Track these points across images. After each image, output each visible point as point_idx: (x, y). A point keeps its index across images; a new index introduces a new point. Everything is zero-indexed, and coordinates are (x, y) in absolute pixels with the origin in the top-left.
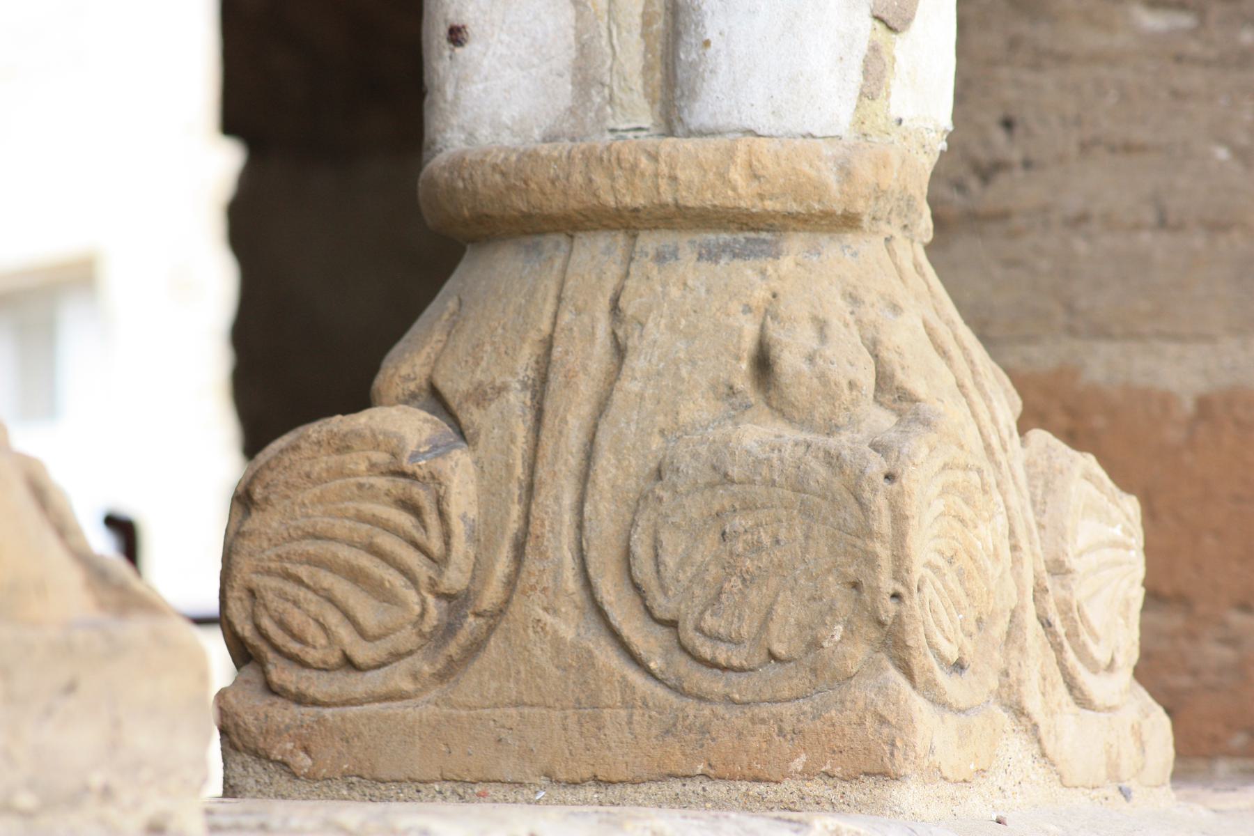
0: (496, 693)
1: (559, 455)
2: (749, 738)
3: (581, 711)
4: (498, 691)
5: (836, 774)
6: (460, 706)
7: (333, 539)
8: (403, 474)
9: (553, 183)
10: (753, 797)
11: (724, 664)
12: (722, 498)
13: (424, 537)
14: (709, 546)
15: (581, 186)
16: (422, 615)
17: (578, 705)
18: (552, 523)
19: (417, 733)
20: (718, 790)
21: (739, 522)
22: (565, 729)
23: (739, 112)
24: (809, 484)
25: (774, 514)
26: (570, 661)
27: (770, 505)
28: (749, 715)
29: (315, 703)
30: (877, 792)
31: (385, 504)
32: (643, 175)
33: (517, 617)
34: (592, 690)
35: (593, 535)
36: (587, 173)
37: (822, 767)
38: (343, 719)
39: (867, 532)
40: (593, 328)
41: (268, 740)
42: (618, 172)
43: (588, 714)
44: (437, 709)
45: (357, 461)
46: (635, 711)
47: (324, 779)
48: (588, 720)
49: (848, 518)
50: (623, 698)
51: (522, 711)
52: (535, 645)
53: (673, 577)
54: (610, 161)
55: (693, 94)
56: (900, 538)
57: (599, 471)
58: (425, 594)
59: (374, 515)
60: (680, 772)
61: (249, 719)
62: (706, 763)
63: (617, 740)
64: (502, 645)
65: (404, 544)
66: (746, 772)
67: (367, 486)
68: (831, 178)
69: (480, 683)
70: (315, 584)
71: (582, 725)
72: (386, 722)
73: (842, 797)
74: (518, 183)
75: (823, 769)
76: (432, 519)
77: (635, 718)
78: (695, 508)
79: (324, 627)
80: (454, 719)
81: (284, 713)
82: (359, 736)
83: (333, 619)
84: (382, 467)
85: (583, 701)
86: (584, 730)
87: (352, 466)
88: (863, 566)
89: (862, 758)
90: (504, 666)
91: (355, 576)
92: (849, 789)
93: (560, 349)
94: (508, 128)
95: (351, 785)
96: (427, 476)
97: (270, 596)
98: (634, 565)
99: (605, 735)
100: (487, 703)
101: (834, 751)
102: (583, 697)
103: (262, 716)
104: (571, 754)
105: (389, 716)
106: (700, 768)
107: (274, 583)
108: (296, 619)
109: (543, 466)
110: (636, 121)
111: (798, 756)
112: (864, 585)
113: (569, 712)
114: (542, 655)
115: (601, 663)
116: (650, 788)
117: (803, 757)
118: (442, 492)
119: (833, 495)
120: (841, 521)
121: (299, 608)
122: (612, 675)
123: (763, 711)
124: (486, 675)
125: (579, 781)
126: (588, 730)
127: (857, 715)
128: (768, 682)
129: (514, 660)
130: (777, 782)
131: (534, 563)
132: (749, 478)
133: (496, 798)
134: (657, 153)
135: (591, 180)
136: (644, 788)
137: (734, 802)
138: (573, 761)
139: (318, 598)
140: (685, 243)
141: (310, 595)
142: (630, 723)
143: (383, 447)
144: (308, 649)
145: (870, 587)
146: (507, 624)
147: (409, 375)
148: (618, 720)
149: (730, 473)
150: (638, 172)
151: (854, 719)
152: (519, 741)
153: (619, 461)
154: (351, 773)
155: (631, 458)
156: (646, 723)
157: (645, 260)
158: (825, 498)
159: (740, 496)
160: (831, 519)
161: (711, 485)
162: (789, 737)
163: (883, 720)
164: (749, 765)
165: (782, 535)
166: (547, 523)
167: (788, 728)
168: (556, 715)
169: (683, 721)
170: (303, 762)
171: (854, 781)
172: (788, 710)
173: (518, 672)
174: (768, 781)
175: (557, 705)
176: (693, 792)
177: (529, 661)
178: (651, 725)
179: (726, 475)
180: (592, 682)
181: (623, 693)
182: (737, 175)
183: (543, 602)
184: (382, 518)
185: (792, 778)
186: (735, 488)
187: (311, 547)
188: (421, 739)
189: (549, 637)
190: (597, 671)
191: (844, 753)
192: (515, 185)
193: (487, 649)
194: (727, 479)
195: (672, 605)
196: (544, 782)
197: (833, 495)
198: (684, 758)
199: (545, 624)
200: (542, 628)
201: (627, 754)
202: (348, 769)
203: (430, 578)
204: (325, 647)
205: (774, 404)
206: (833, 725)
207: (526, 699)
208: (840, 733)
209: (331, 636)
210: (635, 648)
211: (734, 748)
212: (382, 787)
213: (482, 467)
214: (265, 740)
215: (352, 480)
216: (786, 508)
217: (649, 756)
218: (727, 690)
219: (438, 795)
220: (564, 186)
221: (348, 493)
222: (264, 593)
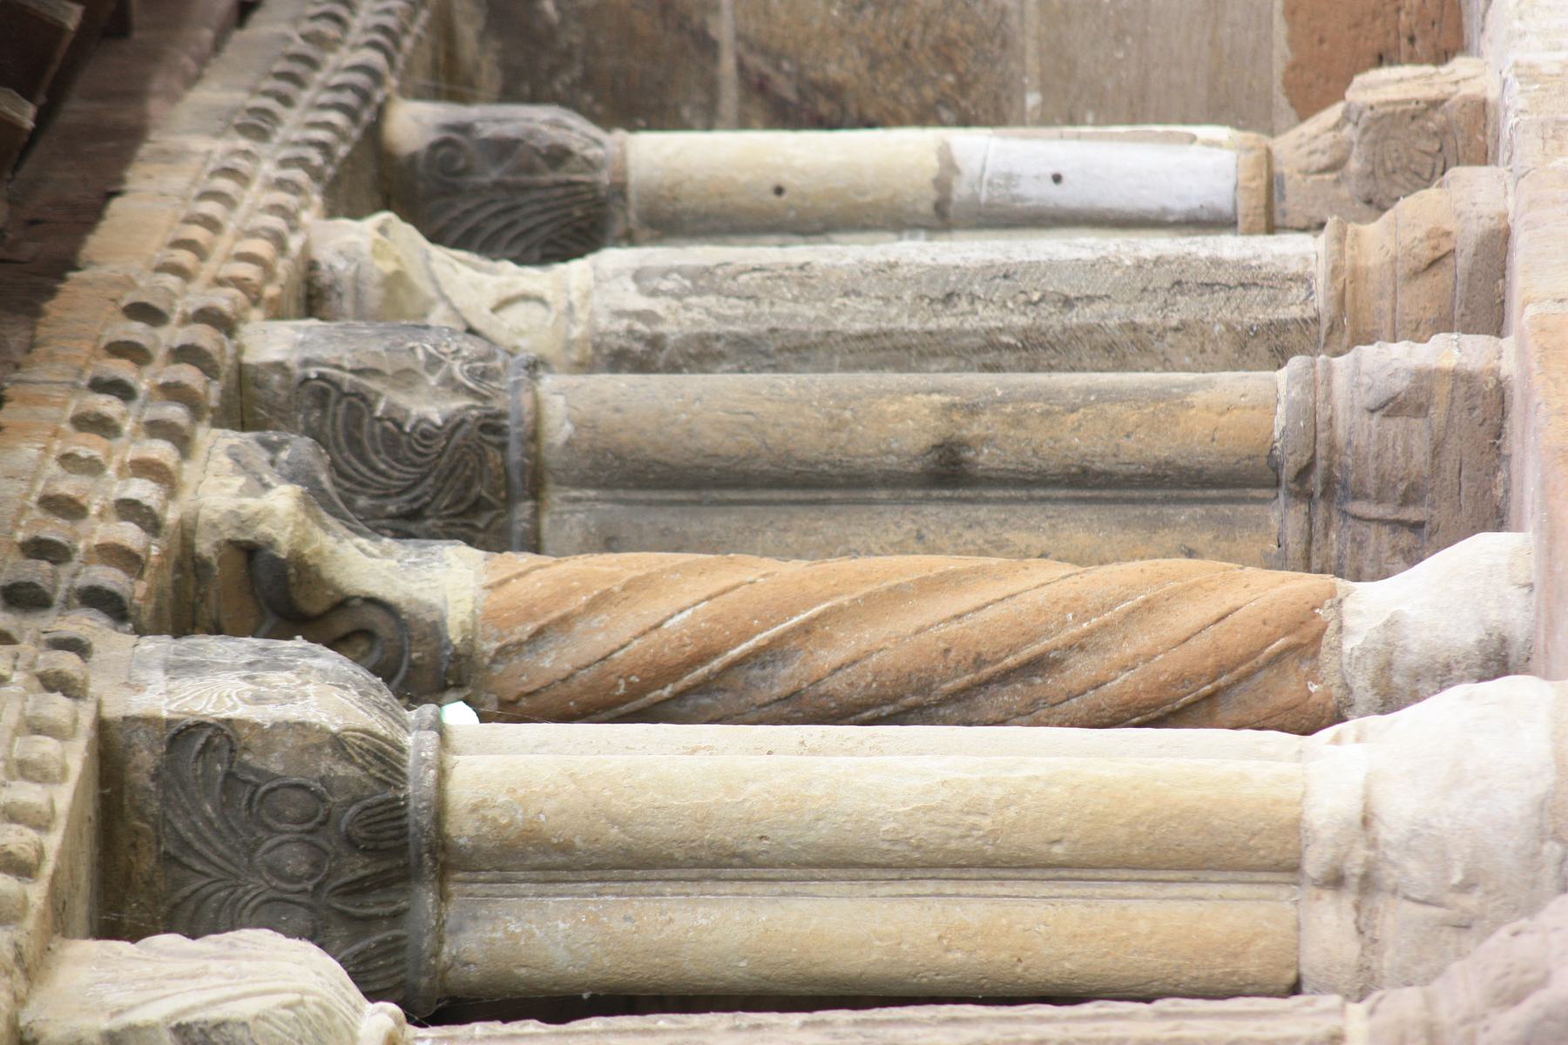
12: (1380, 173)
21: (1389, 165)
39: (1393, 114)
55: (1220, 212)
56: (1395, 103)
68: (1253, 155)
78: (1383, 184)
123: (1461, 153)
125: (1500, 394)
140: (1278, 207)
161: (1375, 179)
163: (1464, 105)
172: (1460, 143)
182: (1253, 185)
194: (1373, 173)
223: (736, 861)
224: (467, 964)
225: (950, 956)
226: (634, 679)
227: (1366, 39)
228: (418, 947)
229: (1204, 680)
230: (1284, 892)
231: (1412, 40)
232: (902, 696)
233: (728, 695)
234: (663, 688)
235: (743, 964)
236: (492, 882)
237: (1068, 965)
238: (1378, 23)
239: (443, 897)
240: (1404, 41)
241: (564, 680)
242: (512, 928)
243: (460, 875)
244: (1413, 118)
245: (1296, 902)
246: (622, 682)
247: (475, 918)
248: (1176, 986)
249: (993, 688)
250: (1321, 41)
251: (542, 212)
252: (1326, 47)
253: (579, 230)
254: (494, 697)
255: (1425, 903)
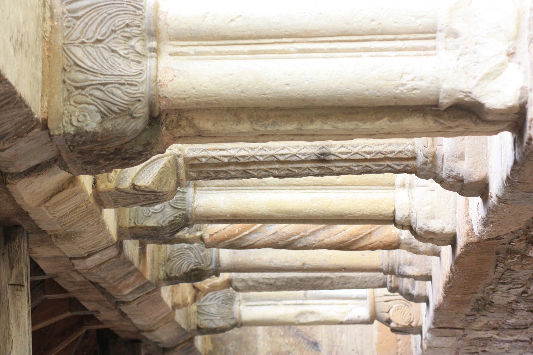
40: (180, 137)
81: (415, 320)
223: (263, 184)
224: (200, 207)
225: (313, 204)
226: (240, 229)
228: (189, 200)
229: (368, 228)
230: (391, 191)
232: (300, 233)
233: (261, 234)
234: (246, 231)
235: (265, 207)
236: (206, 190)
237: (341, 206)
239: (195, 193)
241: (224, 229)
242: (211, 198)
243: (199, 188)
245: (394, 193)
246: (237, 229)
247: (202, 196)
248: (367, 211)
249: (321, 231)
251: (222, 294)
253: (229, 298)
254: (208, 234)
255: (424, 186)
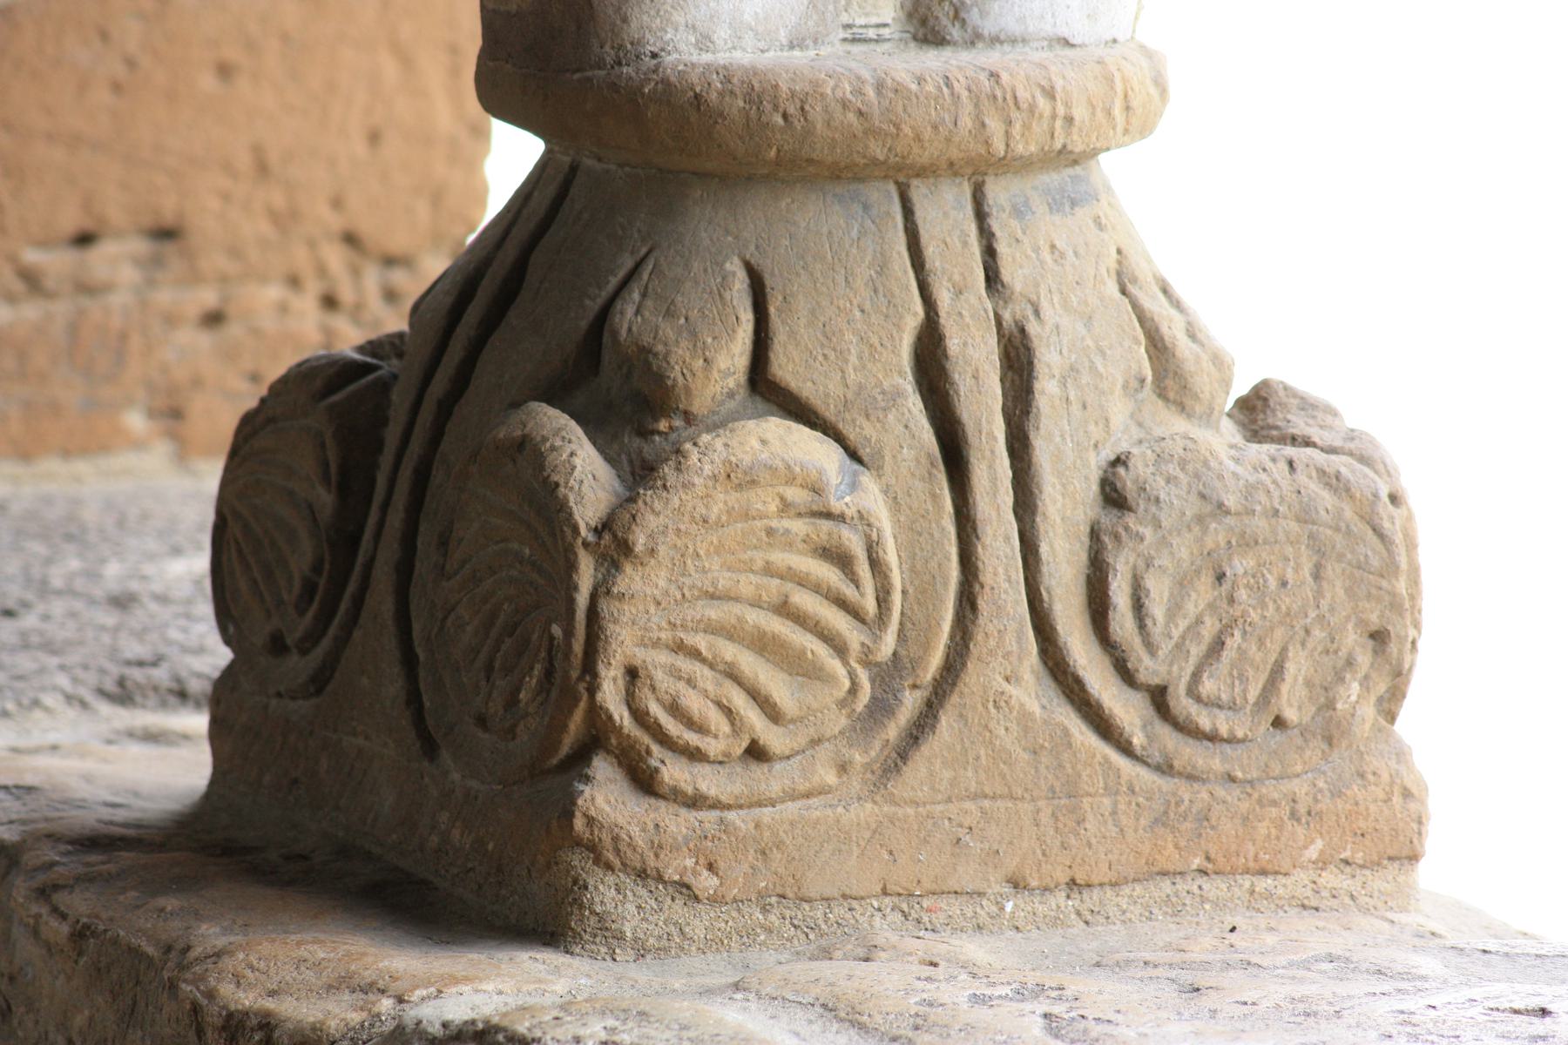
0: (951, 785)
1: (999, 483)
2: (1256, 823)
3: (1056, 802)
4: (954, 782)
5: (1357, 861)
6: (906, 803)
7: (737, 599)
8: (828, 515)
9: (935, 127)
10: (1260, 894)
11: (1225, 736)
12: (1217, 535)
13: (857, 594)
14: (1203, 594)
15: (970, 131)
16: (854, 690)
17: (1053, 794)
18: (1007, 570)
19: (854, 839)
20: (1217, 888)
22: (1037, 825)
23: (1053, 15)
24: (1317, 512)
25: (1279, 551)
26: (1041, 741)
27: (1273, 540)
28: (1256, 795)
29: (717, 805)
30: (1401, 879)
31: (800, 553)
32: (1041, 116)
33: (975, 690)
34: (1068, 776)
35: (1053, 583)
36: (977, 116)
37: (1340, 853)
38: (757, 826)
41: (662, 856)
42: (1015, 114)
43: (1065, 805)
44: (876, 808)
45: (765, 501)
46: (1119, 798)
47: (735, 900)
48: (1064, 812)
49: (1369, 553)
50: (1105, 783)
51: (980, 804)
52: (998, 723)
53: (1163, 633)
54: (1005, 99)
57: (1048, 501)
58: (854, 664)
59: (790, 568)
60: (1171, 868)
61: (635, 831)
62: (1203, 856)
63: (1098, 834)
64: (955, 725)
65: (825, 602)
66: (1251, 864)
67: (781, 531)
69: (931, 774)
70: (714, 658)
71: (1057, 819)
72: (815, 828)
73: (1363, 888)
74: (885, 127)
75: (1342, 856)
76: (863, 570)
77: (1119, 806)
78: (1183, 549)
79: (728, 712)
80: (899, 820)
81: (678, 822)
82: (779, 845)
83: (739, 700)
84: (802, 507)
85: (1058, 789)
86: (1060, 825)
87: (759, 506)
88: (1387, 612)
89: (1387, 839)
90: (959, 750)
91: (763, 645)
92: (1370, 877)
93: (956, 341)
94: (752, 30)
95: (768, 907)
96: (856, 515)
97: (659, 675)
98: (1114, 619)
99: (1085, 829)
100: (940, 797)
101: (1356, 834)
102: (1058, 785)
103: (651, 826)
104: (1044, 854)
105: (818, 819)
106: (1197, 862)
107: (664, 657)
108: (694, 703)
109: (982, 497)
110: (878, 15)
111: (1312, 841)
112: (1392, 635)
113: (1041, 803)
114: (1007, 736)
115: (1079, 742)
116: (1134, 890)
117: (1319, 844)
118: (874, 536)
119: (1348, 526)
120: (1362, 558)
121: (694, 687)
122: (1094, 756)
124: (938, 764)
126: (1065, 825)
127: (1384, 790)
128: (1273, 755)
129: (973, 743)
130: (1286, 874)
131: (991, 621)
132: (1246, 508)
133: (951, 913)
134: (1052, 88)
135: (983, 125)
136: (1126, 890)
137: (1237, 901)
138: (1046, 862)
139: (713, 673)
141: (707, 672)
142: (1114, 813)
143: (799, 481)
144: (708, 739)
145: (1398, 636)
146: (960, 697)
147: (729, 369)
148: (1101, 811)
149: (1226, 503)
150: (1037, 115)
151: (1382, 795)
152: (982, 842)
153: (1064, 485)
154: (770, 892)
155: (1075, 482)
156: (1132, 813)
157: (1004, 216)
158: (1337, 529)
159: (1237, 530)
160: (1349, 556)
161: (1200, 519)
162: (1304, 820)
164: (1256, 856)
165: (1290, 575)
166: (1001, 570)
167: (1302, 810)
168: (1025, 807)
169: (1176, 808)
170: (706, 883)
171: (1375, 868)
173: (978, 758)
174: (1276, 873)
175: (1025, 795)
176: (1188, 892)
177: (991, 743)
178: (1140, 815)
179: (1220, 505)
180: (1068, 765)
181: (1106, 776)
183: (1005, 669)
184: (801, 572)
185: (1302, 867)
186: (1230, 520)
187: (714, 612)
188: (859, 845)
189: (1015, 713)
190: (1075, 753)
191: (1366, 836)
192: (880, 129)
193: (937, 731)
195: (1163, 669)
196: (1006, 890)
197: (1348, 526)
198: (1177, 851)
199: (1010, 697)
200: (1006, 702)
201: (1111, 851)
202: (766, 887)
203: (863, 644)
204: (728, 736)
205: (1171, 395)
206: (1357, 804)
207: (987, 790)
208: (1365, 813)
209: (737, 723)
210: (1119, 722)
211: (1237, 836)
212: (806, 906)
213: (895, 498)
214: (657, 856)
215: (758, 524)
216: (1292, 543)
217: (1137, 852)
218: (1227, 767)
219: (876, 913)
220: (950, 131)
221: (755, 541)
222: (653, 672)
227: (226, 197)
231: (214, 319)
238: (265, 227)
240: (208, 297)
244: (1379, 637)
250: (225, 71)
252: (207, 82)
